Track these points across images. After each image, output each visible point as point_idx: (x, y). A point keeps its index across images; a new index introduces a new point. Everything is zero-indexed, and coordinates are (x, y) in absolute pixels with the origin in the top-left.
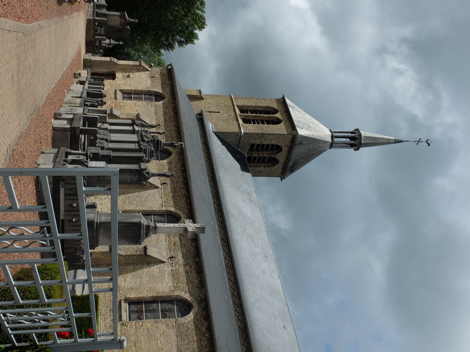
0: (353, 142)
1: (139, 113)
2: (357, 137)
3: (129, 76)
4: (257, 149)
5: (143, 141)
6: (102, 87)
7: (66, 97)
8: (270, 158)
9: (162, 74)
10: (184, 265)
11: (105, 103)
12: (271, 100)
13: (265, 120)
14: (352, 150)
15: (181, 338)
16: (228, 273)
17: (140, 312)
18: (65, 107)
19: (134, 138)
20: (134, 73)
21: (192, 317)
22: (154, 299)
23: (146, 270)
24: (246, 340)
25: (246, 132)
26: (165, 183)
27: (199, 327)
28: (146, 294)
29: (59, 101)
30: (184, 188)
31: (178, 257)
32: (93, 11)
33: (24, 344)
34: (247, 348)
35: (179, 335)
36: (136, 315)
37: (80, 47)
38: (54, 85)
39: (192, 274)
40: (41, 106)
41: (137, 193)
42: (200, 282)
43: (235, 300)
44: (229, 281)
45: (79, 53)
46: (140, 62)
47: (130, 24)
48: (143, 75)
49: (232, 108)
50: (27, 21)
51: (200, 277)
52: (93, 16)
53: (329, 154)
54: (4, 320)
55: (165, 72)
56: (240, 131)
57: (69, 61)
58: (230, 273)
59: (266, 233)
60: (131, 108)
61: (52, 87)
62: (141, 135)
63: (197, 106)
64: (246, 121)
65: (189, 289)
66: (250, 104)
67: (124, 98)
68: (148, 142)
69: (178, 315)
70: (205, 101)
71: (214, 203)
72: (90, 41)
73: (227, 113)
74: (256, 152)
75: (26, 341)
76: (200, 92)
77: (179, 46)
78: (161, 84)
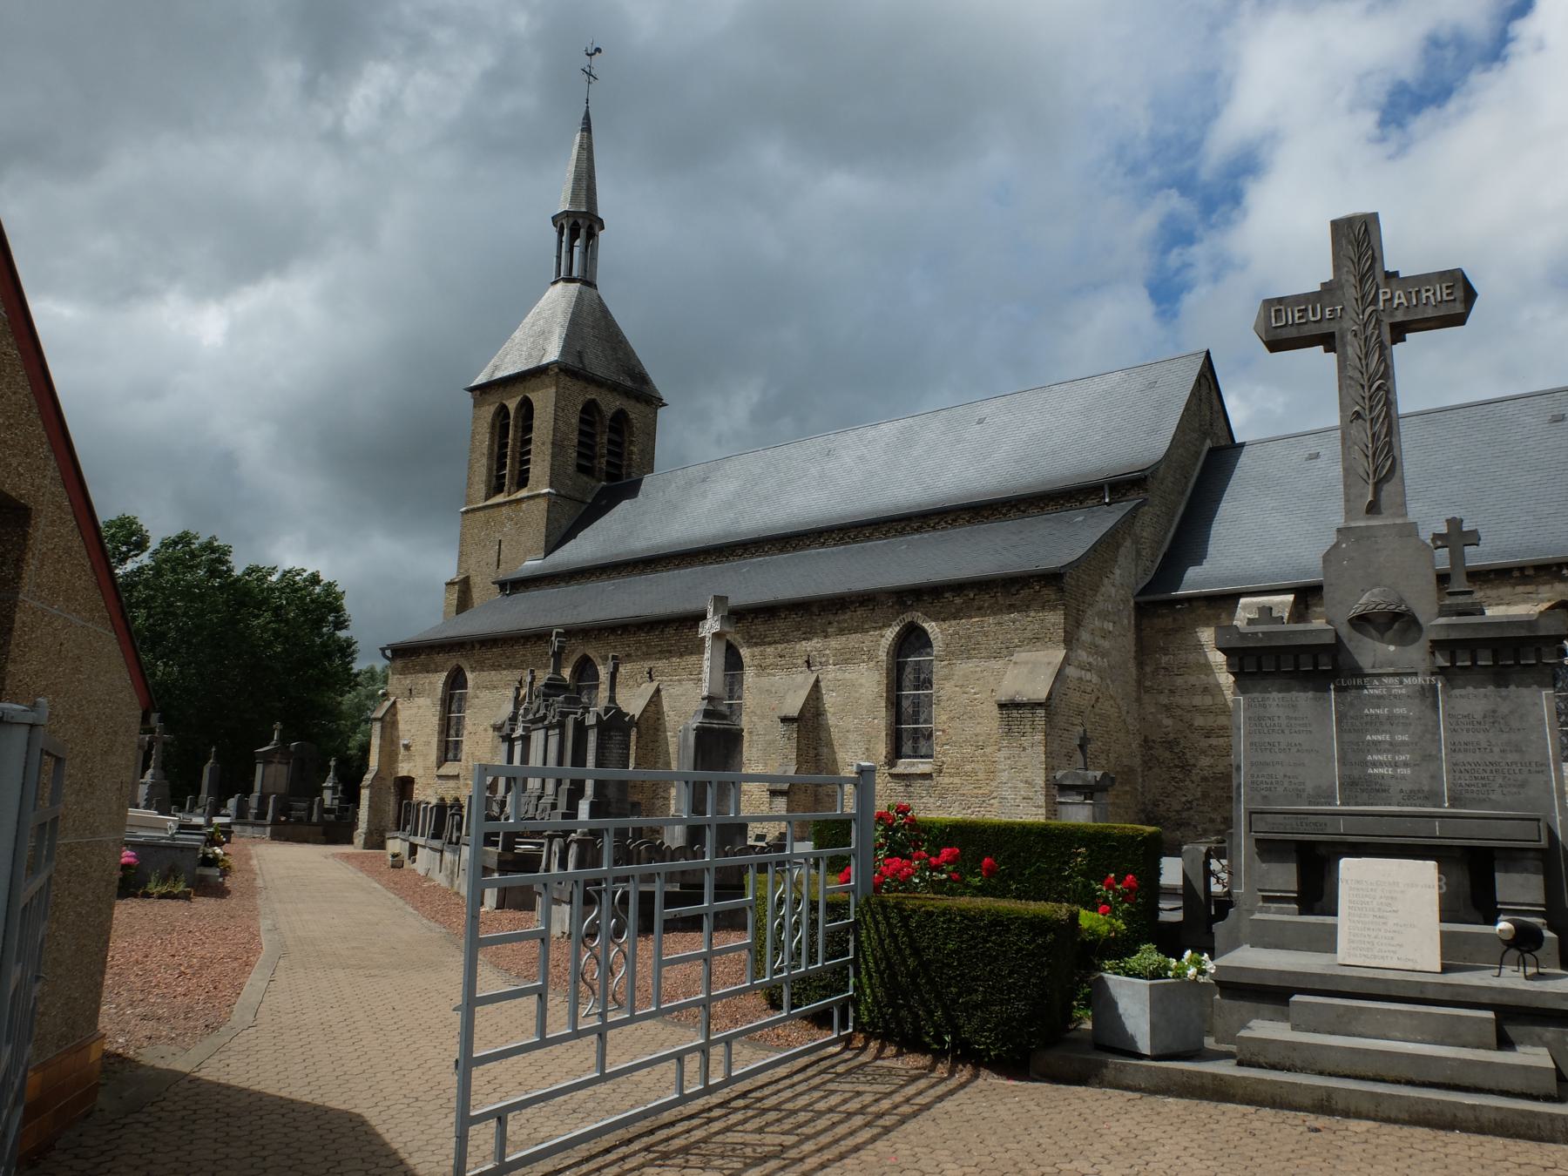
0: (583, 232)
1: (491, 726)
2: (571, 221)
3: (407, 747)
4: (591, 458)
5: (544, 717)
6: (423, 806)
7: (439, 885)
8: (612, 429)
9: (404, 671)
10: (826, 637)
11: (457, 800)
12: (475, 419)
13: (523, 436)
14: (601, 234)
15: (974, 649)
16: (855, 541)
17: (917, 735)
18: (459, 885)
19: (537, 737)
20: (401, 734)
21: (933, 624)
22: (892, 704)
23: (831, 720)
24: (996, 509)
25: (548, 482)
26: (650, 673)
27: (953, 611)
28: (880, 721)
29: (444, 897)
30: (662, 631)
31: (808, 649)
32: (253, 825)
33: (851, 945)
34: (1013, 507)
35: (967, 651)
36: (922, 742)
37: (334, 855)
38: (407, 906)
39: (845, 621)
40: (444, 930)
41: (669, 734)
42: (862, 604)
43: (912, 528)
44: (872, 540)
45: (348, 858)
46: (376, 719)
47: (284, 740)
48: (405, 712)
49: (491, 511)
50: (257, 952)
51: (852, 603)
52: (265, 826)
53: (610, 291)
54: (789, 973)
55: (399, 663)
56: (544, 495)
57: (361, 878)
58: (856, 536)
59: (780, 449)
60: (480, 742)
61: (411, 910)
62: (533, 722)
63: (483, 591)
64: (522, 481)
65: (875, 629)
66: (484, 470)
67: (457, 759)
68: (547, 706)
69: (929, 654)
70: (472, 573)
71: (703, 563)
72: (324, 834)
73: (503, 524)
74: (596, 462)
75: (847, 941)
76: (450, 584)
77: (346, 627)
78: (426, 675)
